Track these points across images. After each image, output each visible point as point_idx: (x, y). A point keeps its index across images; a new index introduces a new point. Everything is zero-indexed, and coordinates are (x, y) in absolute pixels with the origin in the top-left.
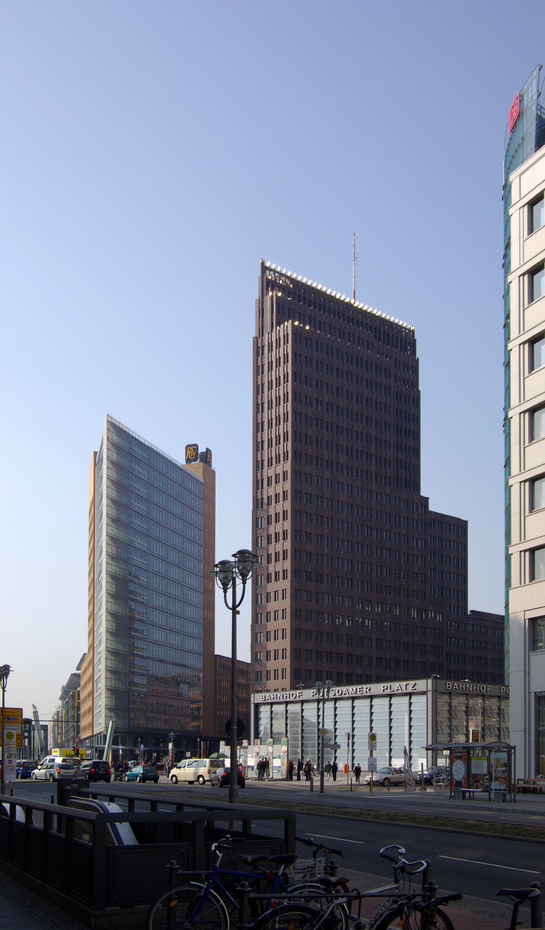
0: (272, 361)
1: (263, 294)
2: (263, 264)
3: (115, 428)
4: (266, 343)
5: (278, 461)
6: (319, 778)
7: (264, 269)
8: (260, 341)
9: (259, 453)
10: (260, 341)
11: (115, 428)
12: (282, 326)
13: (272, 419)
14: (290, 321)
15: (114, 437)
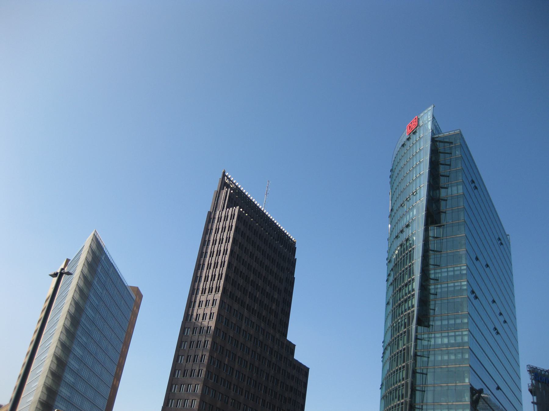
0: (212, 288)
1: (221, 188)
2: (224, 173)
3: (96, 241)
4: (217, 217)
5: (210, 291)
6: (198, 311)
7: (224, 175)
8: (213, 215)
9: (197, 284)
10: (213, 215)
11: (96, 241)
12: (231, 209)
13: (211, 264)
14: (238, 207)
15: (94, 247)
